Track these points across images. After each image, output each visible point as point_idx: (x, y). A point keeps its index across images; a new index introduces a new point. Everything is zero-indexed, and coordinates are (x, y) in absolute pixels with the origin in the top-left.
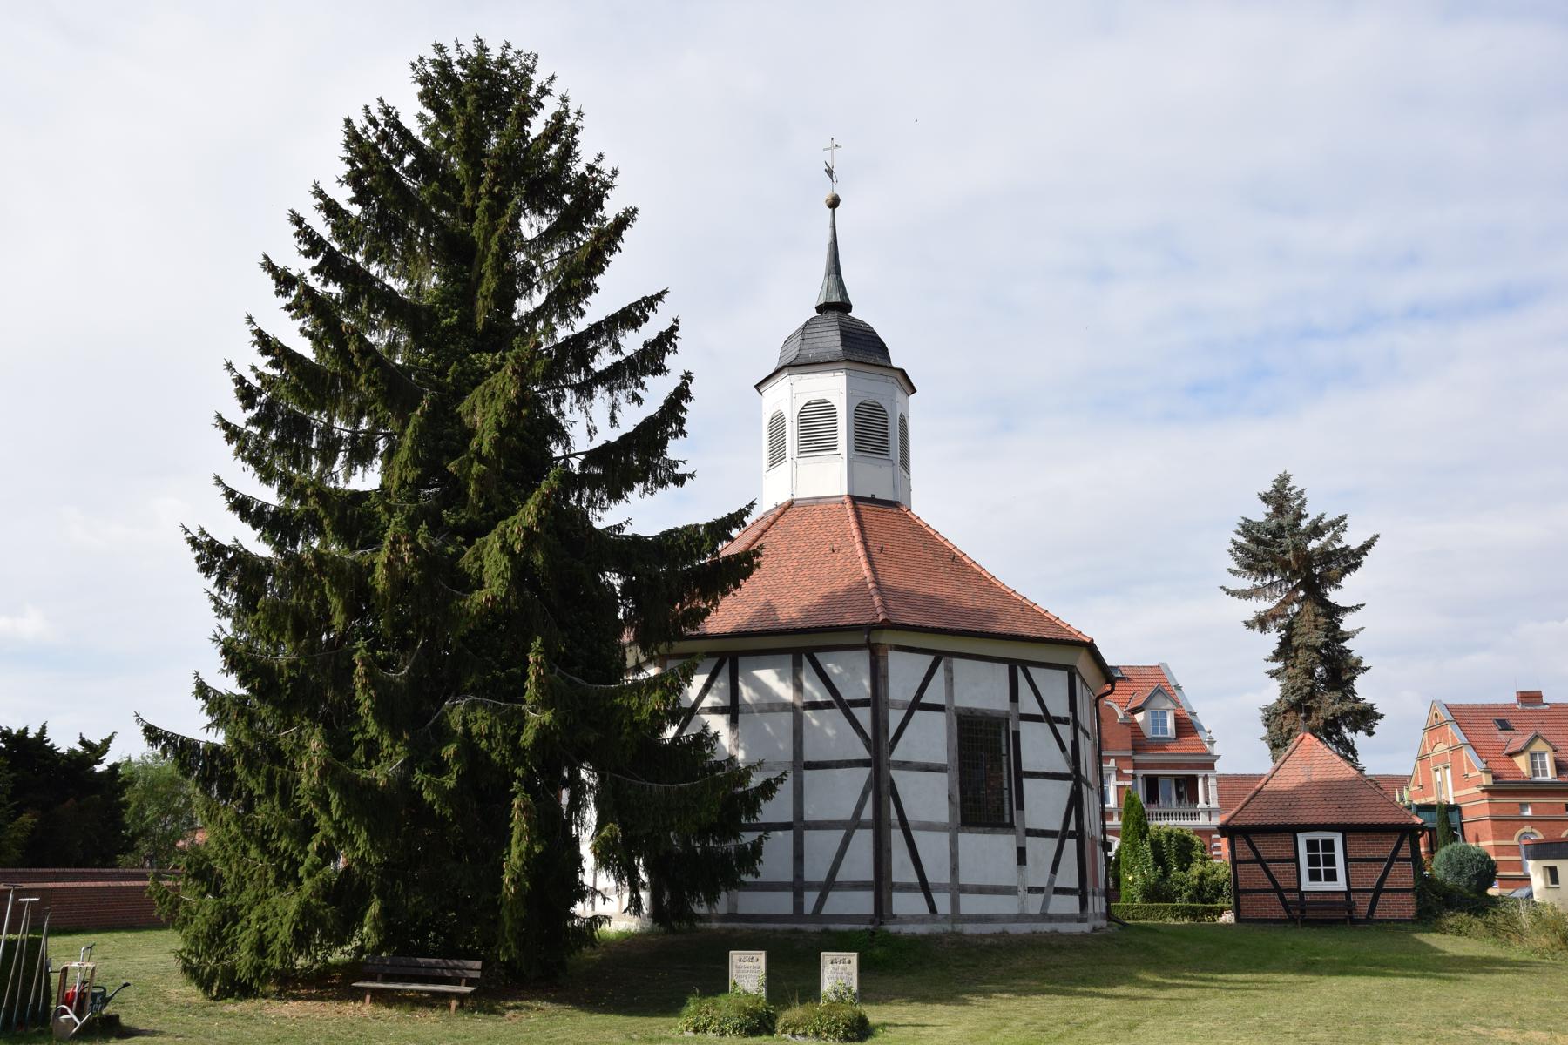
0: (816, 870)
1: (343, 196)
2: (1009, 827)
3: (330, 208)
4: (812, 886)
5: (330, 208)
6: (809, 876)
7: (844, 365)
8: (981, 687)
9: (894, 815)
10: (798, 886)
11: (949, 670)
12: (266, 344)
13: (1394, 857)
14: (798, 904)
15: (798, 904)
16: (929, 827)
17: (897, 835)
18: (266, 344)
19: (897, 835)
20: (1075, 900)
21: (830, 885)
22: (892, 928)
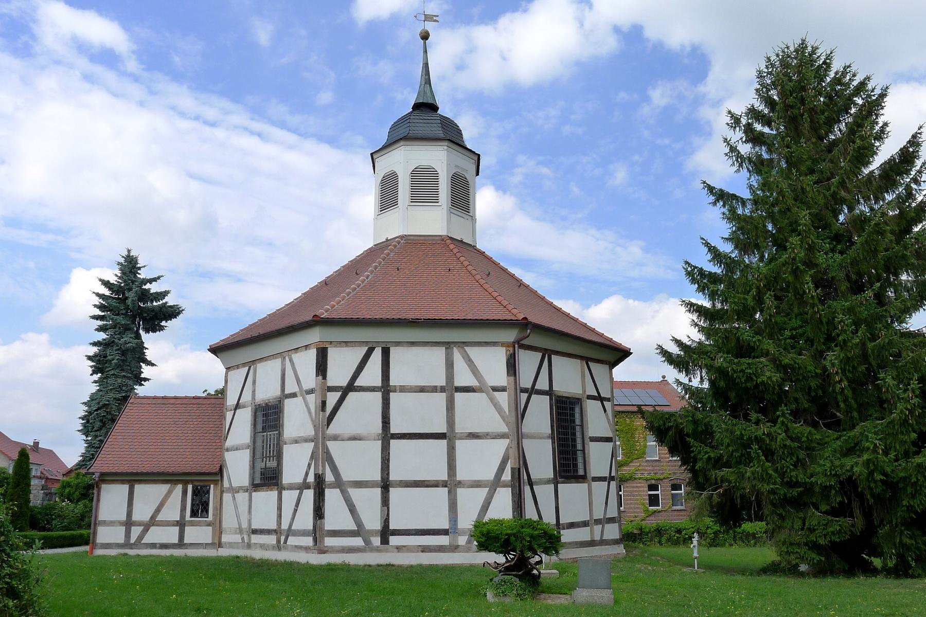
0: (142, 513)
1: (727, 248)
2: (583, 478)
3: (717, 256)
4: (139, 524)
5: (717, 256)
6: (135, 517)
7: (446, 143)
8: (568, 377)
9: (525, 477)
10: (129, 523)
11: (291, 360)
12: (98, 295)
13: (147, 527)
14: (128, 534)
15: (128, 534)
16: (359, 484)
17: (527, 489)
18: (98, 295)
19: (527, 489)
20: (311, 539)
21: (153, 522)
22: (99, 552)
